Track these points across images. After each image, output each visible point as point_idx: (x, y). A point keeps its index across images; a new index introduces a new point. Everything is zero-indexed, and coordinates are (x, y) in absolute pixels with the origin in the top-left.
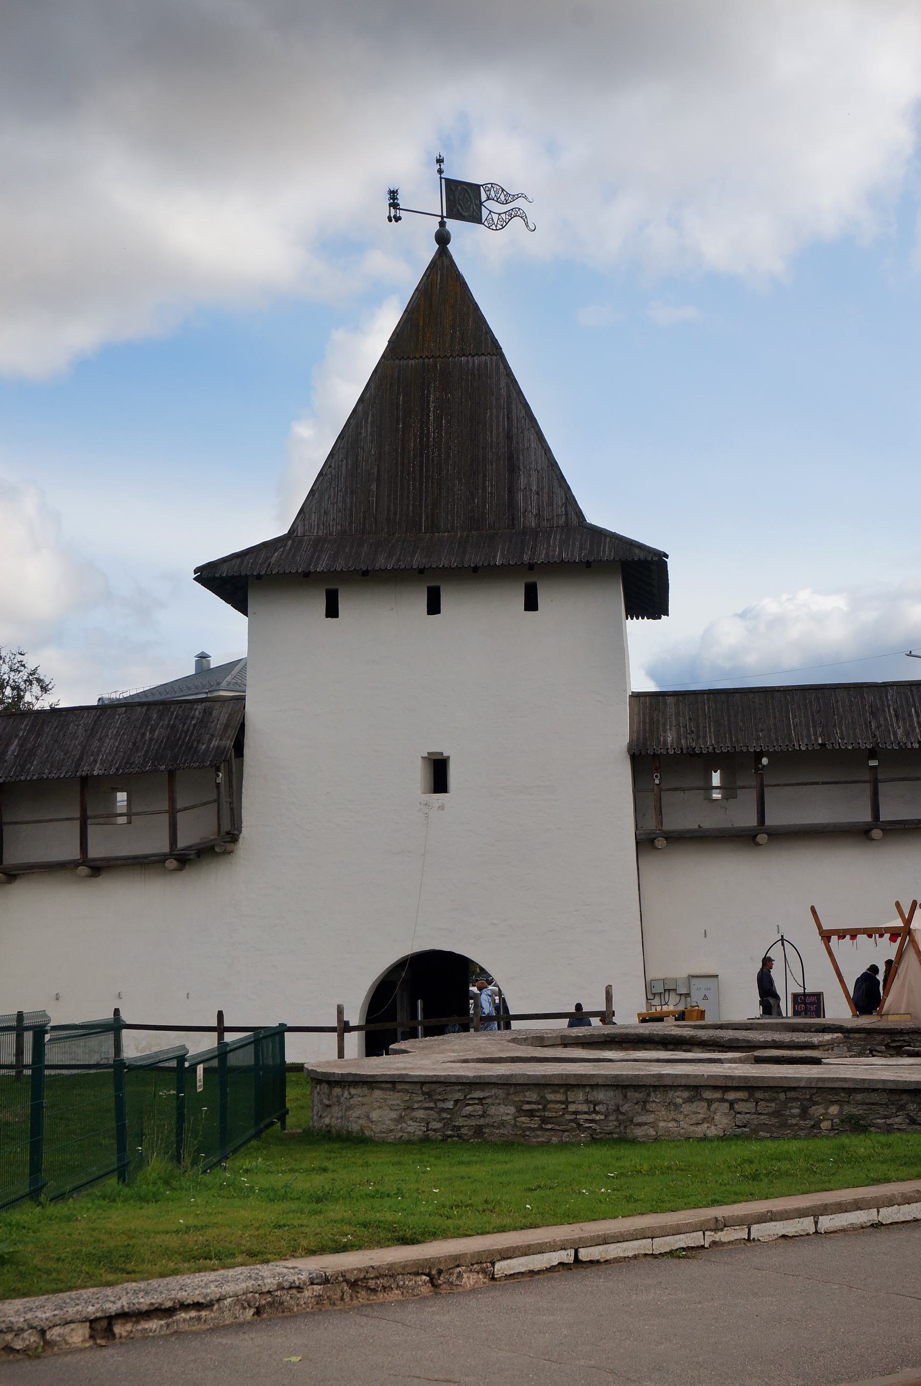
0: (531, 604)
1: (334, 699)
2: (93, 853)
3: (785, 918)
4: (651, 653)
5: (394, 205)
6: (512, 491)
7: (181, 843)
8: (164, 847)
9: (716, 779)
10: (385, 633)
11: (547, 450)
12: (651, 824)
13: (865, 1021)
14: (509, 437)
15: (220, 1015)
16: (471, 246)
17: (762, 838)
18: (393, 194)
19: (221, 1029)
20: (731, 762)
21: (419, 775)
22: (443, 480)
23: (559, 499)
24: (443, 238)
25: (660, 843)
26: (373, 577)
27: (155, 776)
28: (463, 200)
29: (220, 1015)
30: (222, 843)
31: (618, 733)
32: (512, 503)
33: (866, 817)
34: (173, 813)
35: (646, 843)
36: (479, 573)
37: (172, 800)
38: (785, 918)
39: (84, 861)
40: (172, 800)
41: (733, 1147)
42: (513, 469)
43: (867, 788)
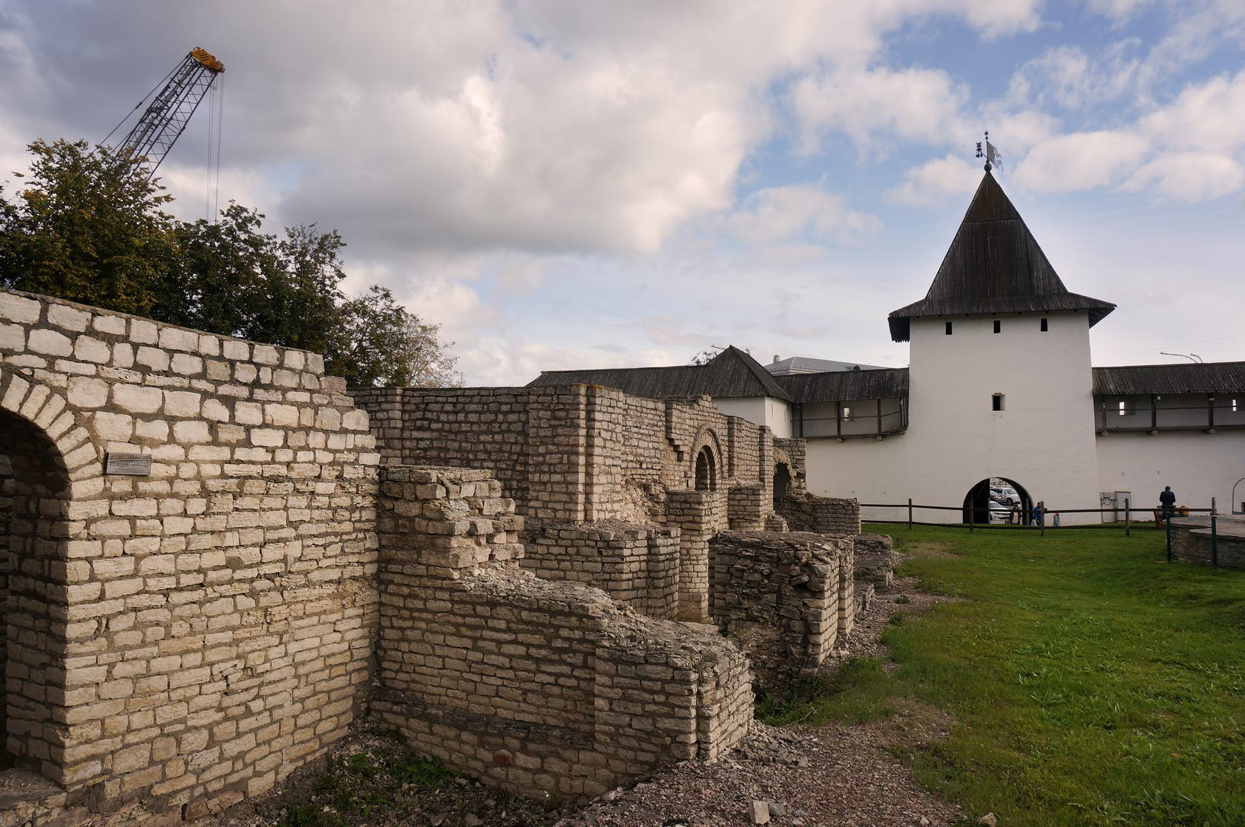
0: (997, 330)
1: (961, 370)
3: (1146, 472)
4: (1110, 346)
6: (1030, 278)
8: (876, 431)
9: (1122, 405)
11: (1046, 260)
13: (734, 533)
14: (1027, 255)
20: (1142, 401)
21: (1006, 402)
23: (1054, 281)
25: (1106, 433)
26: (970, 316)
27: (862, 402)
30: (899, 429)
31: (1088, 384)
33: (1149, 424)
34: (879, 417)
35: (1099, 433)
38: (1146, 472)
41: (503, 585)
42: (1030, 269)
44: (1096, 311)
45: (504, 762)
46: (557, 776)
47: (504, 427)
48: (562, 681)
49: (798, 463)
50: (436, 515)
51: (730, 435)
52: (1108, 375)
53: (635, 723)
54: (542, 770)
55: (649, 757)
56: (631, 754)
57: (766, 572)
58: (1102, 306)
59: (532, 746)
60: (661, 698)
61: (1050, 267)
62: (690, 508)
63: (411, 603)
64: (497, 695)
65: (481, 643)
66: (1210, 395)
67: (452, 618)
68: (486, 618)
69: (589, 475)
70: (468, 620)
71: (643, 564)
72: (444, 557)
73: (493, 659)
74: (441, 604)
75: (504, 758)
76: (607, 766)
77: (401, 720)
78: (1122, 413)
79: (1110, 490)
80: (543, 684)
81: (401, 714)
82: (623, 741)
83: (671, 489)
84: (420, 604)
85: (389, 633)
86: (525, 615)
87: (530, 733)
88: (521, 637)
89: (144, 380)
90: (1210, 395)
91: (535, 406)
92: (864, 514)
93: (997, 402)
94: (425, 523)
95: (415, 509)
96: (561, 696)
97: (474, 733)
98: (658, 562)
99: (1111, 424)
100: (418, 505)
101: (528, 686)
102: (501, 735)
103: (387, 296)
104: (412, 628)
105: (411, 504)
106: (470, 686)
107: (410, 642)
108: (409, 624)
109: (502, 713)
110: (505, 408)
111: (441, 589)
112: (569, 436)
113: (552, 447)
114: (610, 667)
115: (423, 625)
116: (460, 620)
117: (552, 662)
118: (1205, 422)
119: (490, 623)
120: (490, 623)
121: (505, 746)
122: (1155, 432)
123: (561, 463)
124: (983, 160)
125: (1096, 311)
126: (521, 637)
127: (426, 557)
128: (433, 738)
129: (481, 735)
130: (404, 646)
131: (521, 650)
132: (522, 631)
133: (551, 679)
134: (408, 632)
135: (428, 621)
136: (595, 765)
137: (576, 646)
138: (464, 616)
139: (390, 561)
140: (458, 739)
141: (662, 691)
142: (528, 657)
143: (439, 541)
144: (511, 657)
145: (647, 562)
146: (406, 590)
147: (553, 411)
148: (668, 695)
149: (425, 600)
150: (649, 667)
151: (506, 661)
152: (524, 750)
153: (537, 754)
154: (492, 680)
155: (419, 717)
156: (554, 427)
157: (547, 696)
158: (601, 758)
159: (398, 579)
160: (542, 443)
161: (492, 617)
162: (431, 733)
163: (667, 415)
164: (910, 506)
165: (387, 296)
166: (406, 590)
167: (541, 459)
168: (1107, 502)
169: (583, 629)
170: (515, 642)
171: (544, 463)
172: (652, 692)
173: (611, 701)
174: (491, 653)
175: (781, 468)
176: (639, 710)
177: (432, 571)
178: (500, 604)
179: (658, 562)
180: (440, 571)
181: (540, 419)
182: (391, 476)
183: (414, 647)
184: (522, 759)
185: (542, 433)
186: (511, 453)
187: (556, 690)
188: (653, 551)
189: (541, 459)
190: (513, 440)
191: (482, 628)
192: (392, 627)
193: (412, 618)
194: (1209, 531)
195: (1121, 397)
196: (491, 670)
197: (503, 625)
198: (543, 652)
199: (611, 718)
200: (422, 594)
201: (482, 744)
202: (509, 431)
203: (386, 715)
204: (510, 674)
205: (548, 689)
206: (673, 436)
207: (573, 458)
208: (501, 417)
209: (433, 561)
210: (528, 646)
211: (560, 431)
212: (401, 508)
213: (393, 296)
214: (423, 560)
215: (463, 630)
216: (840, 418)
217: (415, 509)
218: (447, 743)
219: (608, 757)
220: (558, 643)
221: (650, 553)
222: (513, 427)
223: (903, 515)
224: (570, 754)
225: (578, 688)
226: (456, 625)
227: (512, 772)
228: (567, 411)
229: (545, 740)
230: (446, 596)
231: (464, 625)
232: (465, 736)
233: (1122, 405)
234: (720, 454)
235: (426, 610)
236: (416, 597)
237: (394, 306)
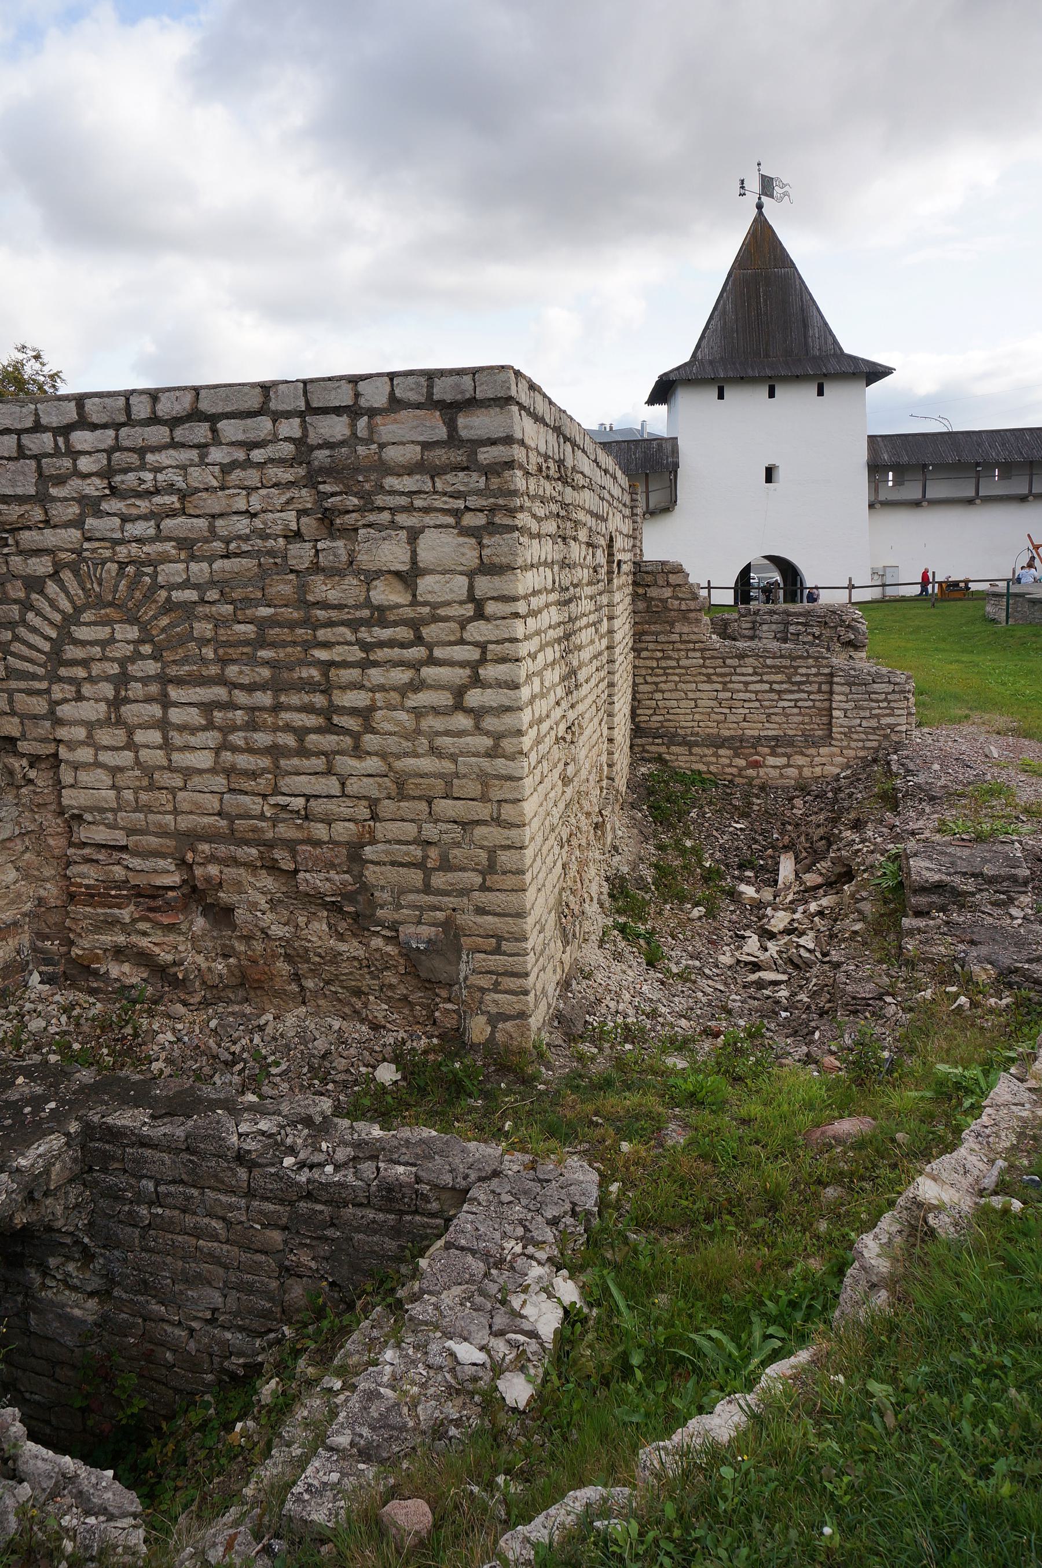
0: (772, 395)
3: (975, 545)
4: (889, 409)
5: (742, 188)
6: (806, 337)
10: (747, 405)
11: (822, 317)
14: (803, 310)
15: (850, 580)
16: (772, 212)
19: (851, 587)
20: (918, 467)
21: (781, 475)
22: (767, 331)
23: (830, 340)
24: (760, 206)
25: (878, 506)
26: (743, 380)
28: (767, 185)
29: (850, 580)
30: (668, 507)
31: (861, 454)
32: (806, 344)
33: (973, 494)
35: (871, 506)
36: (797, 379)
37: (647, 487)
39: (247, 511)
40: (647, 487)
44: (875, 373)
45: (756, 765)
46: (800, 768)
48: (799, 704)
50: (689, 596)
52: (881, 444)
53: (865, 723)
54: (788, 766)
55: (875, 744)
56: (860, 744)
57: (817, 634)
58: (881, 370)
59: (780, 750)
60: (885, 704)
61: (826, 324)
63: (663, 664)
64: (744, 720)
65: (730, 686)
66: (978, 464)
67: (704, 671)
68: (735, 668)
70: (718, 670)
73: (742, 696)
74: (695, 660)
75: (757, 762)
76: (842, 754)
77: (663, 749)
78: (890, 484)
80: (784, 708)
81: (663, 744)
82: (855, 736)
84: (674, 663)
85: (643, 688)
86: (769, 662)
87: (776, 744)
88: (765, 678)
90: (978, 464)
93: (770, 474)
95: (667, 593)
96: (800, 714)
97: (729, 748)
100: (670, 590)
101: (772, 711)
102: (754, 747)
103: (37, 357)
104: (665, 682)
106: (721, 717)
107: (663, 692)
108: (663, 678)
109: (749, 732)
111: (694, 650)
114: (846, 689)
115: (677, 678)
116: (711, 671)
117: (792, 692)
118: (971, 493)
119: (738, 670)
120: (738, 670)
121: (757, 754)
122: (978, 501)
124: (752, 199)
126: (765, 678)
127: (678, 627)
128: (693, 758)
129: (735, 749)
130: (658, 696)
131: (767, 687)
132: (767, 673)
133: (792, 704)
134: (662, 685)
135: (680, 675)
136: (832, 755)
137: (812, 679)
138: (714, 668)
140: (716, 755)
141: (885, 700)
142: (772, 690)
143: (692, 615)
144: (756, 692)
146: (659, 654)
148: (889, 702)
149: (678, 660)
150: (875, 686)
151: (753, 696)
152: (773, 754)
153: (784, 755)
154: (741, 711)
155: (679, 745)
157: (787, 716)
158: (836, 750)
159: (651, 646)
161: (740, 666)
162: (691, 754)
165: (37, 357)
166: (659, 654)
168: (876, 577)
169: (818, 667)
170: (761, 681)
172: (878, 701)
173: (846, 711)
174: (739, 691)
176: (867, 714)
177: (685, 637)
178: (748, 656)
180: (693, 637)
182: (643, 569)
183: (667, 695)
184: (771, 761)
187: (796, 711)
191: (731, 674)
192: (646, 683)
193: (666, 674)
195: (891, 468)
196: (739, 704)
197: (750, 670)
198: (785, 686)
199: (846, 722)
200: (675, 655)
201: (737, 755)
203: (647, 747)
204: (757, 704)
205: (788, 711)
209: (686, 629)
210: (771, 683)
212: (653, 592)
213: (45, 358)
214: (677, 630)
215: (714, 678)
217: (667, 593)
218: (704, 759)
219: (842, 748)
220: (798, 678)
224: (812, 751)
225: (814, 707)
226: (708, 675)
227: (762, 771)
229: (791, 744)
230: (698, 654)
231: (715, 674)
232: (721, 752)
235: (679, 667)
236: (670, 658)
237: (46, 370)
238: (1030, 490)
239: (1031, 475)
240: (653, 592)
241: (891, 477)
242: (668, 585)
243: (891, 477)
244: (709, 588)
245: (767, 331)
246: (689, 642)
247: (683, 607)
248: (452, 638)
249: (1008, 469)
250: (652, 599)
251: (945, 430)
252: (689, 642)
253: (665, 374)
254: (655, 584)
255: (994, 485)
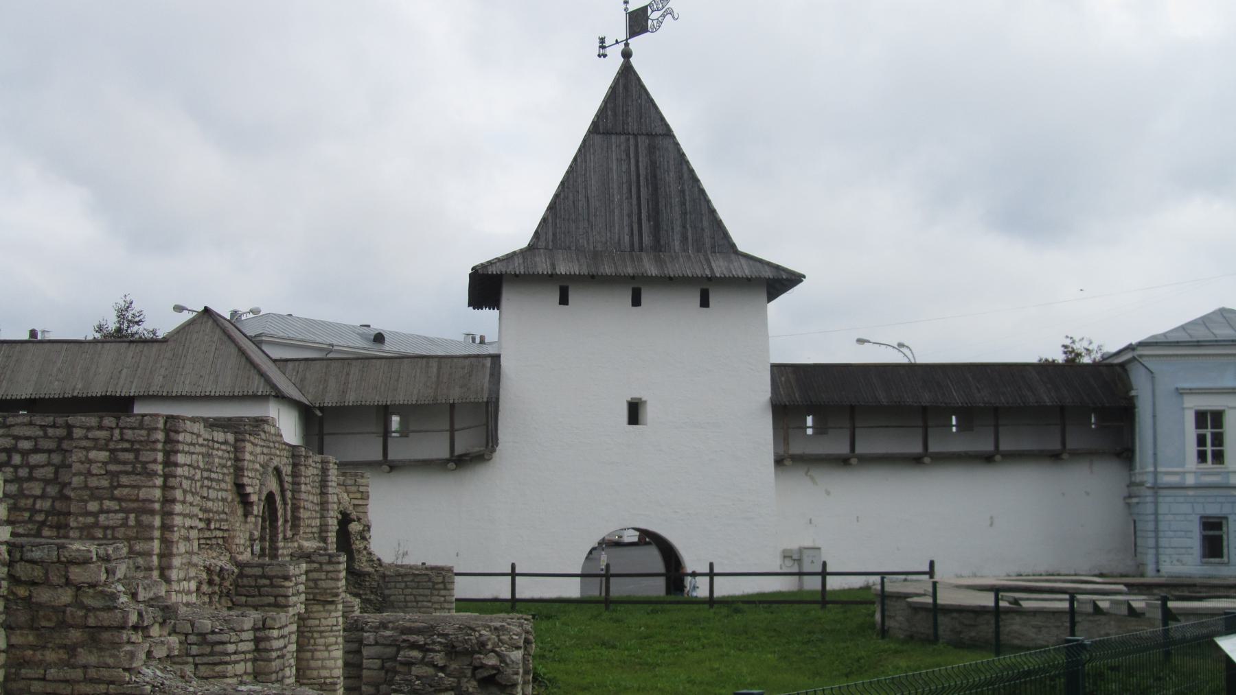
1: (559, 365)
2: (392, 456)
4: (803, 332)
5: (603, 47)
7: (456, 453)
8: (445, 454)
9: (809, 420)
12: (781, 452)
15: (711, 565)
17: (998, 457)
18: (602, 40)
20: (845, 414)
21: (650, 413)
25: (788, 462)
29: (711, 565)
31: (763, 390)
34: (452, 431)
35: (779, 462)
43: (920, 431)
44: (779, 281)
47: (23, 473)
49: (361, 507)
51: (295, 475)
62: (272, 585)
69: (166, 542)
71: (249, 665)
72: (112, 656)
78: (810, 432)
79: (794, 545)
83: (240, 558)
89: (1072, 601)
91: (84, 443)
92: (463, 588)
93: (635, 412)
94: (81, 613)
95: (66, 597)
98: (270, 660)
99: (796, 448)
105: (60, 590)
110: (26, 445)
112: (139, 487)
113: (108, 504)
118: (917, 449)
123: (125, 524)
125: (779, 281)
139: (25, 663)
143: (106, 636)
145: (255, 660)
147: (112, 451)
156: (114, 475)
160: (93, 497)
163: (236, 449)
164: (513, 574)
167: (90, 520)
168: (788, 562)
171: (96, 525)
175: (345, 520)
177: (92, 673)
179: (270, 660)
180: (105, 673)
181: (90, 462)
185: (93, 482)
186: (33, 511)
188: (262, 645)
189: (90, 520)
190: (38, 492)
194: (929, 600)
202: (31, 478)
206: (246, 480)
207: (145, 519)
208: (17, 459)
209: (92, 659)
211: (124, 480)
212: (43, 595)
216: (386, 433)
217: (66, 597)
221: (257, 650)
222: (39, 473)
223: (501, 588)
228: (137, 452)
233: (809, 420)
234: (285, 504)
238: (997, 446)
239: (996, 427)
240: (43, 595)
241: (954, 422)
242: (68, 583)
243: (954, 422)
244: (712, 574)
245: (633, 216)
246: (99, 681)
247: (91, 621)
248: (993, 622)
249: (970, 416)
250: (40, 605)
251: (905, 361)
252: (99, 681)
253: (484, 266)
254: (46, 582)
255: (952, 436)
